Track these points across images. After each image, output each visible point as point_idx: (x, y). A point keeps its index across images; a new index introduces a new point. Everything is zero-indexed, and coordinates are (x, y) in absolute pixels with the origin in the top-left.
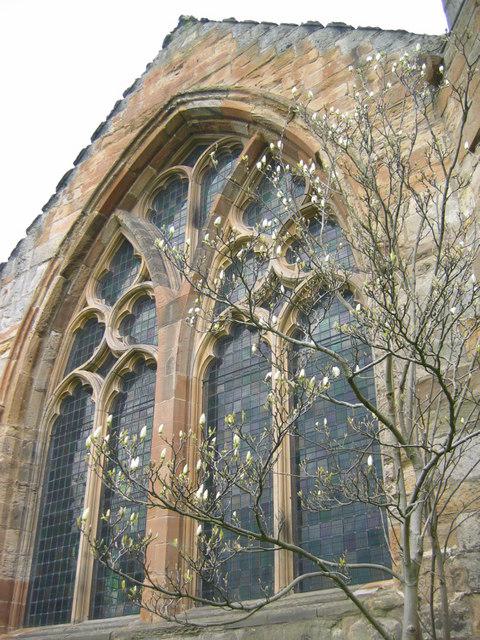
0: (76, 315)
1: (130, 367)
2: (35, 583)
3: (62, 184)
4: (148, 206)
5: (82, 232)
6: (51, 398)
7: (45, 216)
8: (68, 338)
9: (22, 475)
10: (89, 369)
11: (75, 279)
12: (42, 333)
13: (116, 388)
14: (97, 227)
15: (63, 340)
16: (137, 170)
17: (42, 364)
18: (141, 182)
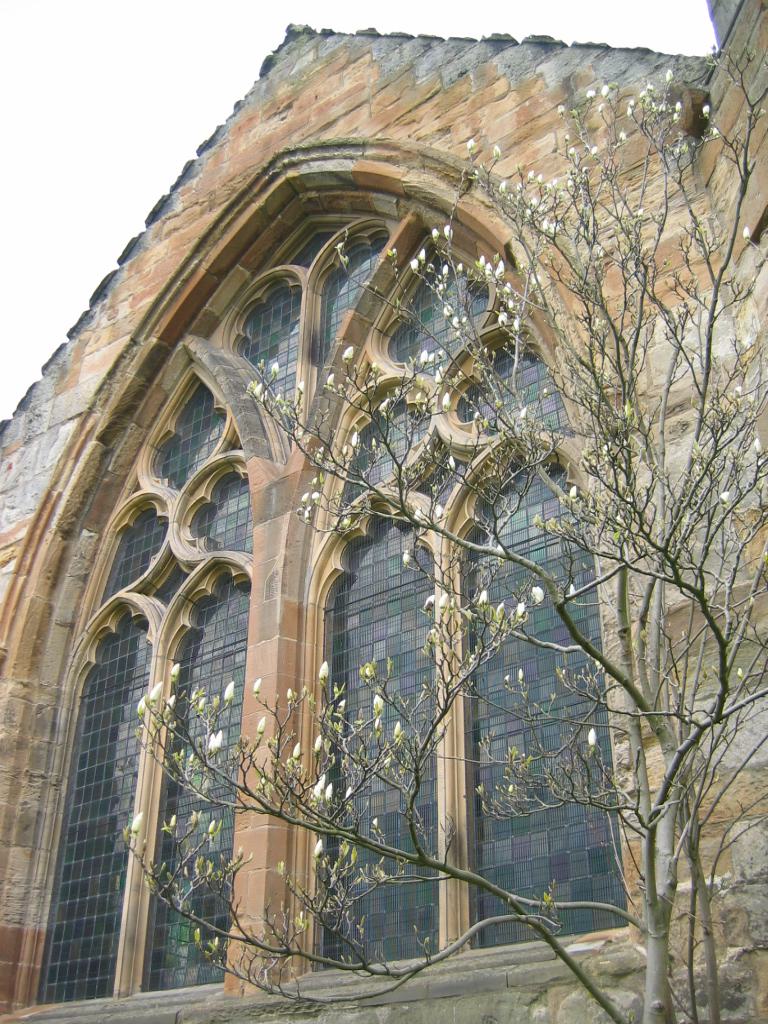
0: (121, 505)
1: (208, 587)
2: (55, 933)
3: (99, 294)
4: (238, 330)
5: (130, 372)
6: (82, 637)
7: (72, 345)
8: (109, 542)
9: (35, 760)
10: (143, 590)
11: (121, 446)
12: (67, 533)
13: (185, 620)
14: (155, 362)
15: (101, 544)
16: (219, 272)
17: (67, 582)
18: (225, 291)
